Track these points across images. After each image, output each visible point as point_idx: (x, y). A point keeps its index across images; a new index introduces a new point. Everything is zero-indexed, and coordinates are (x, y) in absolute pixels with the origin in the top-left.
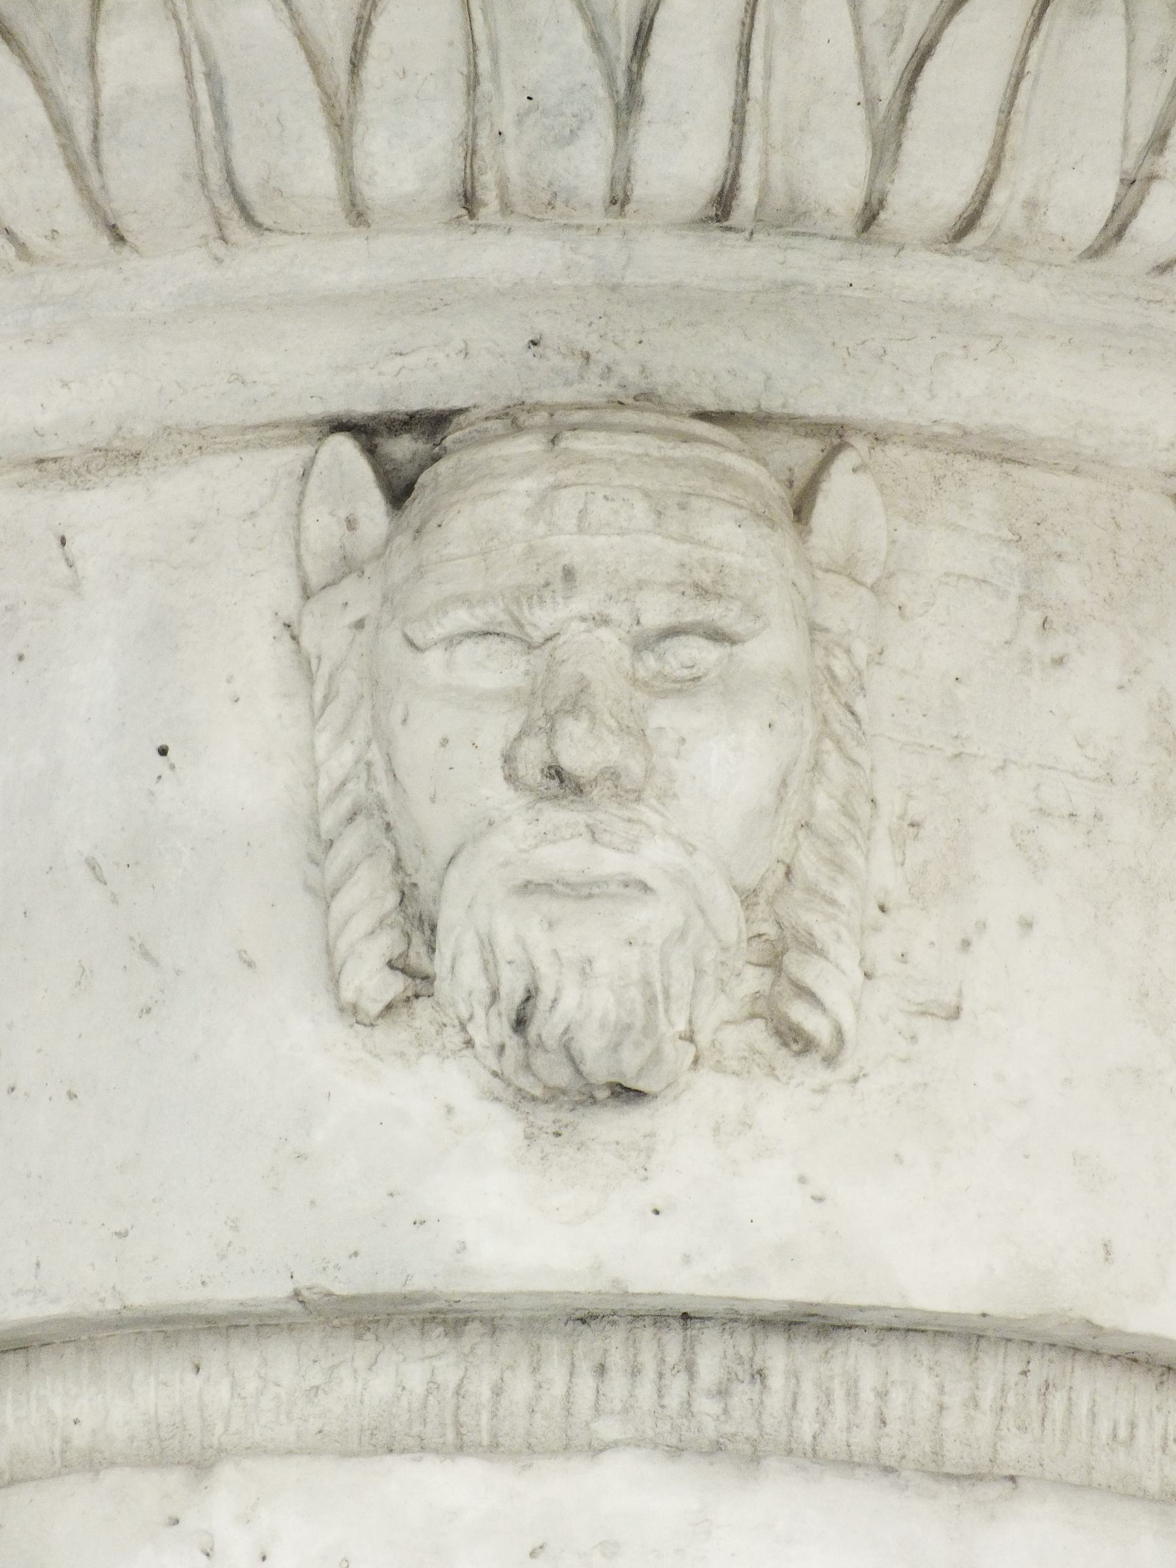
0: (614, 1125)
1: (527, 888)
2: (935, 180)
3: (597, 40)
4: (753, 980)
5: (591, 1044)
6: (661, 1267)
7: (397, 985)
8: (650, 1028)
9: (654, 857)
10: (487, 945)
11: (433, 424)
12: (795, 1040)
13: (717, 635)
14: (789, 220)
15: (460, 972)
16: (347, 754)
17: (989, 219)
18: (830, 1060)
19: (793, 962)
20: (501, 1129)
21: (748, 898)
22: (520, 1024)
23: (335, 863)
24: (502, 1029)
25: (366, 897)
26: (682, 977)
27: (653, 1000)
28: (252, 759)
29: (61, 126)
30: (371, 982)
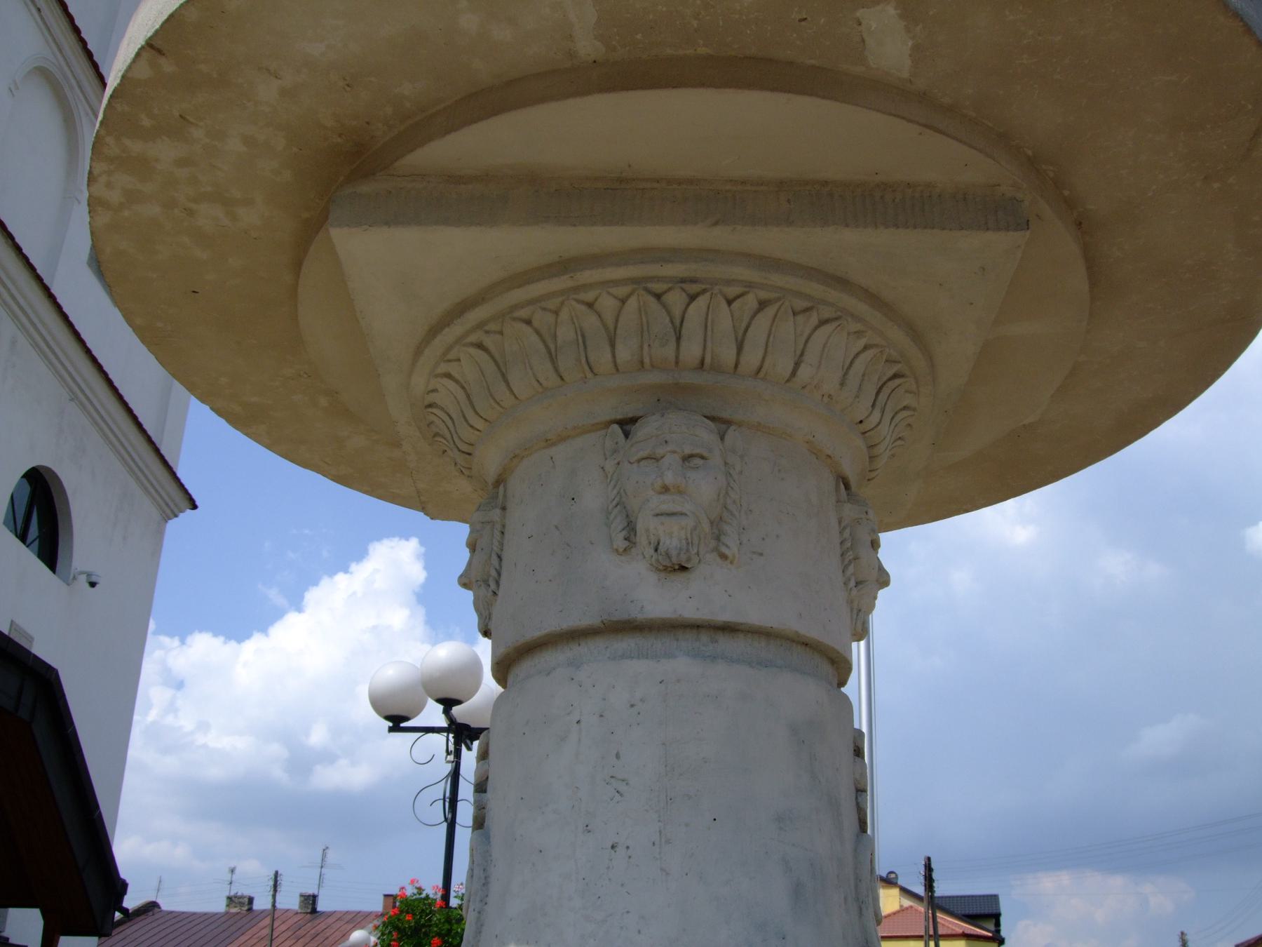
0: (682, 576)
1: (657, 515)
2: (752, 357)
3: (672, 322)
4: (713, 543)
5: (674, 553)
6: (690, 612)
7: (627, 543)
8: (688, 550)
9: (687, 507)
10: (647, 530)
11: (634, 420)
12: (724, 557)
13: (702, 457)
14: (717, 369)
15: (642, 539)
16: (615, 492)
17: (764, 370)
18: (731, 563)
19: (722, 538)
20: (652, 577)
21: (712, 523)
22: (656, 550)
23: (612, 517)
24: (652, 551)
25: (619, 523)
26: (696, 541)
27: (689, 543)
28: (593, 497)
29: (549, 352)
30: (620, 543)
